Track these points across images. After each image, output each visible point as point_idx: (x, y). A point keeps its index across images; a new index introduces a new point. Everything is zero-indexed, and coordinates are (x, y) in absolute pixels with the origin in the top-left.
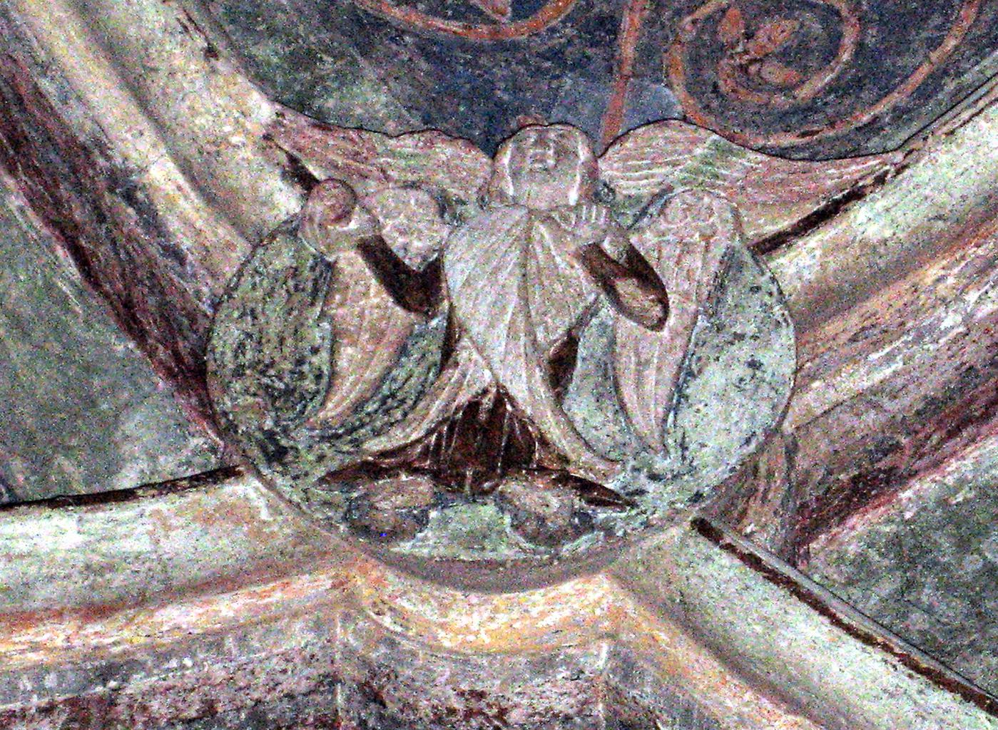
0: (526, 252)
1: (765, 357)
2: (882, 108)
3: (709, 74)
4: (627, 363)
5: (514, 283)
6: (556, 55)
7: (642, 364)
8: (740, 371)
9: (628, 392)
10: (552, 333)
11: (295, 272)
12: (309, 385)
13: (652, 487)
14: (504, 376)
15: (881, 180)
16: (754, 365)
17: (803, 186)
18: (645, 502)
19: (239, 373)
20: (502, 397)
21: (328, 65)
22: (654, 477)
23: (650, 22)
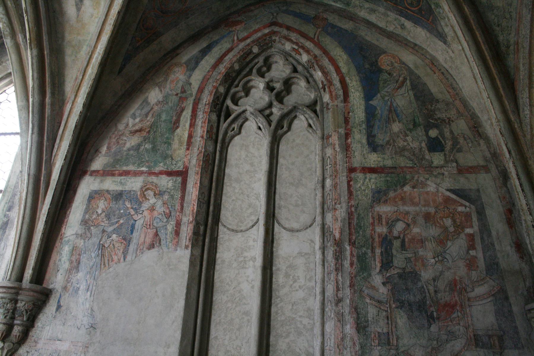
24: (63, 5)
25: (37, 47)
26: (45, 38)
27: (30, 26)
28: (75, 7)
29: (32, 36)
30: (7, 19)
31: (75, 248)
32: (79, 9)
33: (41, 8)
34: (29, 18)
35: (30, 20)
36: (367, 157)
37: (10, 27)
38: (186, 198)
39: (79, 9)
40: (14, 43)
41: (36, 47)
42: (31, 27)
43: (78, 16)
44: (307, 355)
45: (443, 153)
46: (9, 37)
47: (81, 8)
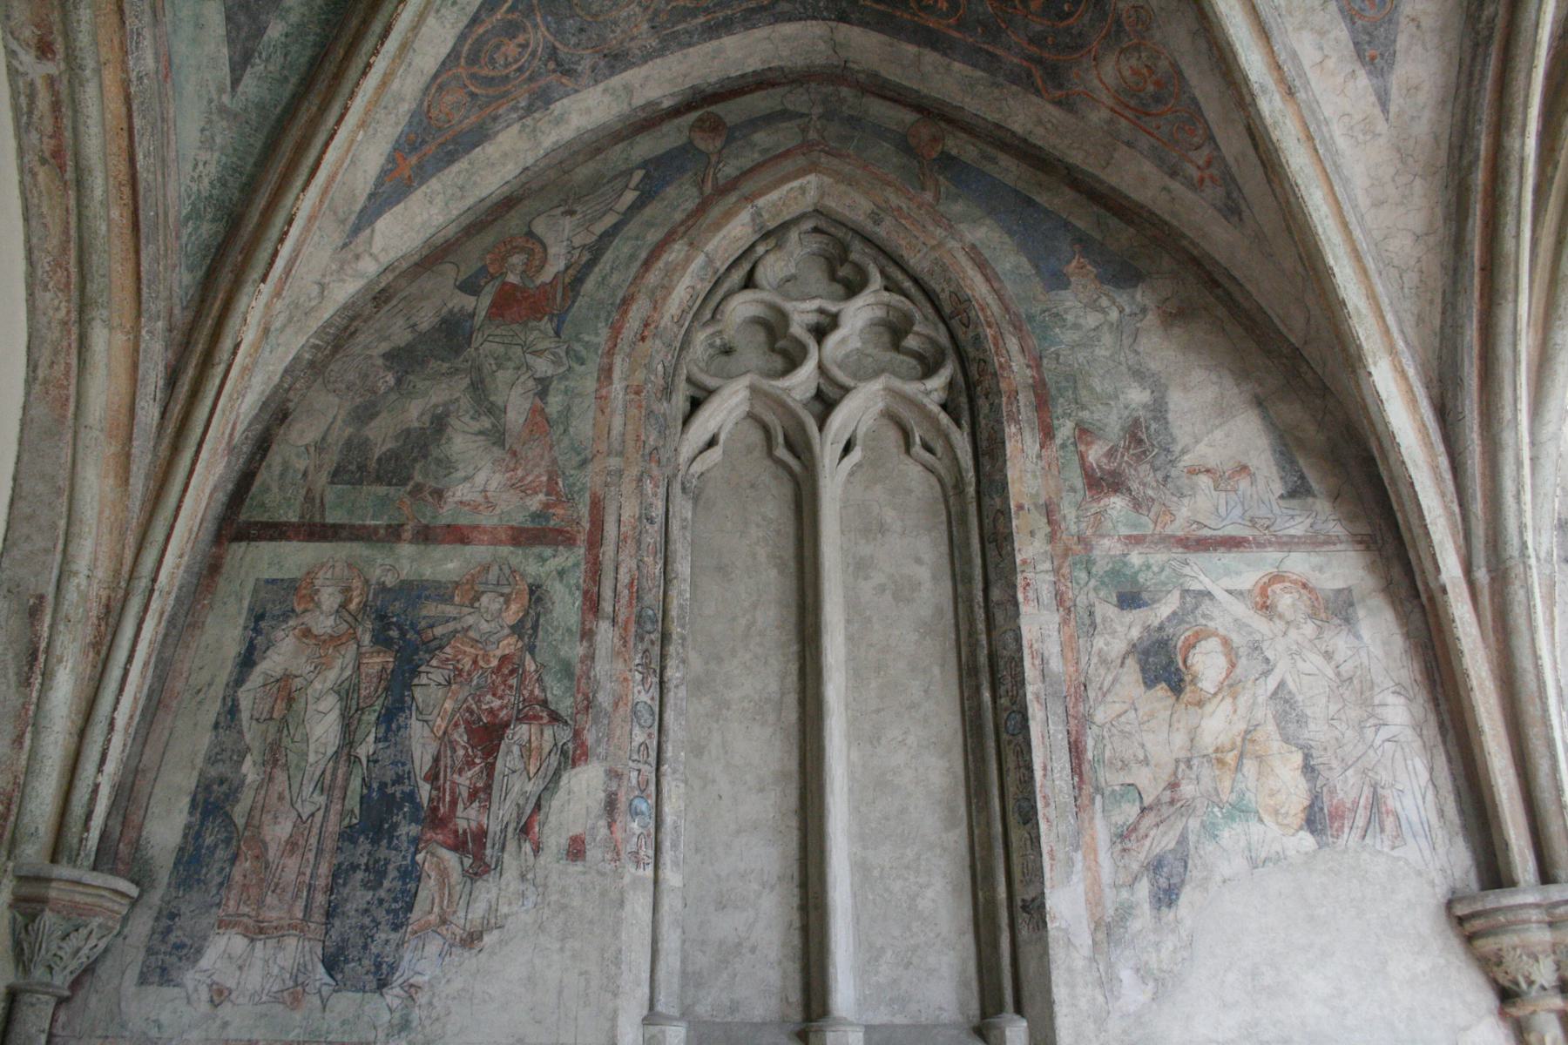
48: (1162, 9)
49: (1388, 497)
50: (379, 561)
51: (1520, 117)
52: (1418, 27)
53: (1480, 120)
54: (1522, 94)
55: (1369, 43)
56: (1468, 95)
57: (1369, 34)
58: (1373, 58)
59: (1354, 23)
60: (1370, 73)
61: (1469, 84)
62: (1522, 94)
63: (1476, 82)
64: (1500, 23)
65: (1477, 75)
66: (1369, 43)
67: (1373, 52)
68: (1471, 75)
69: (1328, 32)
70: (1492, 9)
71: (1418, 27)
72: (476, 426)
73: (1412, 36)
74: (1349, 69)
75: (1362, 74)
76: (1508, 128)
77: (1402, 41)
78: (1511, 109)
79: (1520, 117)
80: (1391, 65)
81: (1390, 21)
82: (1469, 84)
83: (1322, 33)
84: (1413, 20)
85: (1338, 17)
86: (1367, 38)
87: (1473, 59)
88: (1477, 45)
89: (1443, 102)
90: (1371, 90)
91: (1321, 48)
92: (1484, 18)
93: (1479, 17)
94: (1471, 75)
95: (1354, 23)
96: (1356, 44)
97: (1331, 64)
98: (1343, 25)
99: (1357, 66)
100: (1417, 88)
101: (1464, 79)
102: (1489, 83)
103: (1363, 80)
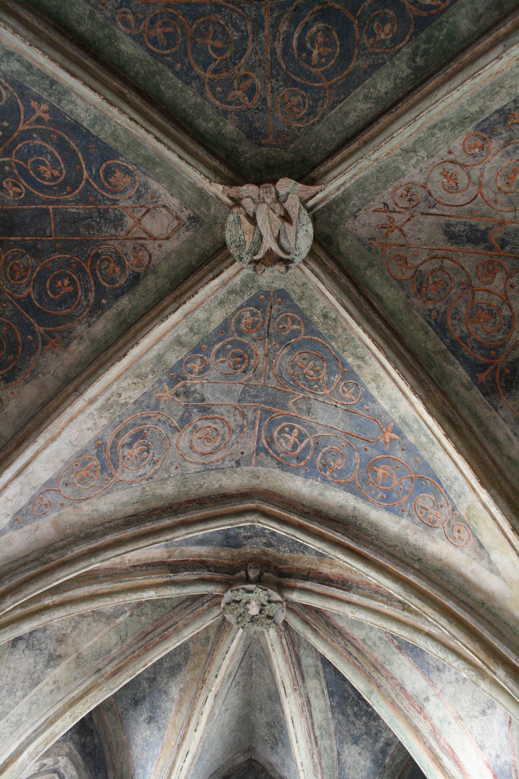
0: (269, 217)
1: (308, 229)
2: (315, 120)
3: (284, 110)
4: (288, 232)
5: (269, 225)
6: (257, 109)
7: (290, 232)
8: (305, 232)
9: (289, 238)
10: (276, 235)
11: (234, 220)
12: (242, 243)
13: (296, 257)
14: (271, 246)
15: (321, 190)
16: (307, 231)
17: (309, 192)
18: (296, 261)
19: (231, 244)
20: (271, 249)
21: (221, 124)
22: (296, 255)
23: (272, 98)
24: (483, 587)
25: (498, 664)
26: (496, 643)
27: (470, 648)
28: (492, 575)
29: (481, 658)
30: (463, 662)
31: (109, 669)
32: (498, 573)
33: (463, 616)
34: (462, 640)
35: (464, 642)
36: (480, 268)
37: (472, 668)
38: (303, 663)
39: (498, 573)
40: (490, 682)
41: (496, 666)
42: (472, 649)
43: (504, 580)
44: (494, 776)
45: (444, 24)
46: (480, 681)
47: (497, 568)
48: (6, 414)
49: (125, 685)
50: (396, 414)
51: (20, 597)
52: (35, 530)
53: (10, 581)
54: (30, 591)
55: (23, 515)
56: (16, 569)
57: (27, 513)
58: (17, 520)
59: (29, 504)
60: (10, 522)
61: (22, 566)
62: (30, 591)
63: (24, 569)
64: (52, 564)
65: (27, 567)
66: (23, 515)
67: (19, 519)
68: (25, 564)
69: (23, 495)
70: (55, 557)
71: (35, 530)
72: (375, 407)
73: (31, 530)
74: (10, 512)
75: (9, 519)
76: (14, 594)
77: (27, 527)
78: (22, 591)
79: (20, 597)
80: (17, 529)
81: (34, 518)
82: (22, 566)
83: (21, 494)
84: (38, 527)
85: (30, 496)
86: (25, 513)
87: (32, 561)
88: (38, 559)
89: (8, 558)
90: (3, 527)
91: (15, 496)
92: (50, 555)
93: (49, 553)
94: (25, 564)
95: (29, 504)
96: (21, 510)
97: (10, 504)
98: (27, 500)
99: (12, 515)
100: (10, 544)
101: (21, 562)
102: (27, 574)
103: (6, 521)
